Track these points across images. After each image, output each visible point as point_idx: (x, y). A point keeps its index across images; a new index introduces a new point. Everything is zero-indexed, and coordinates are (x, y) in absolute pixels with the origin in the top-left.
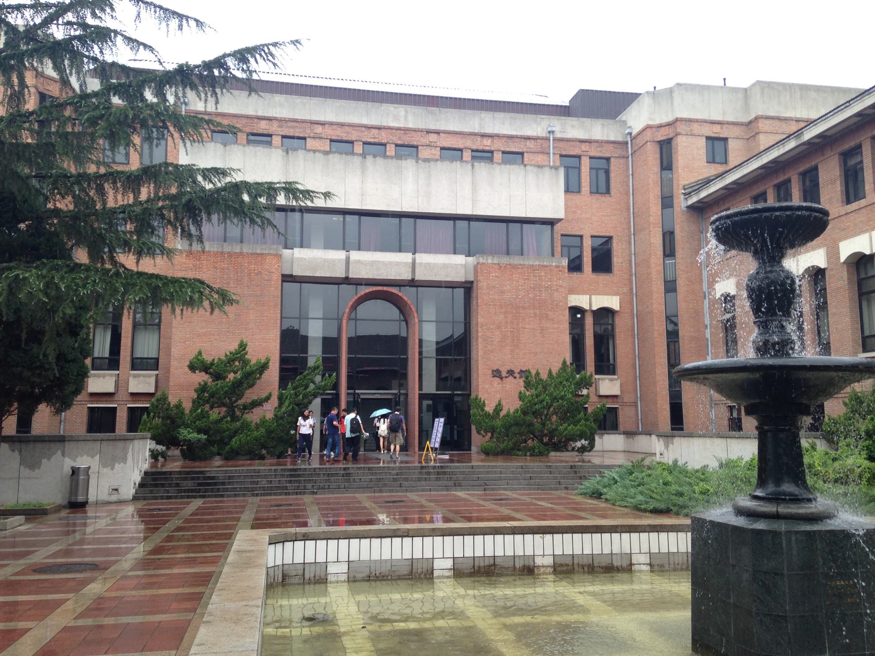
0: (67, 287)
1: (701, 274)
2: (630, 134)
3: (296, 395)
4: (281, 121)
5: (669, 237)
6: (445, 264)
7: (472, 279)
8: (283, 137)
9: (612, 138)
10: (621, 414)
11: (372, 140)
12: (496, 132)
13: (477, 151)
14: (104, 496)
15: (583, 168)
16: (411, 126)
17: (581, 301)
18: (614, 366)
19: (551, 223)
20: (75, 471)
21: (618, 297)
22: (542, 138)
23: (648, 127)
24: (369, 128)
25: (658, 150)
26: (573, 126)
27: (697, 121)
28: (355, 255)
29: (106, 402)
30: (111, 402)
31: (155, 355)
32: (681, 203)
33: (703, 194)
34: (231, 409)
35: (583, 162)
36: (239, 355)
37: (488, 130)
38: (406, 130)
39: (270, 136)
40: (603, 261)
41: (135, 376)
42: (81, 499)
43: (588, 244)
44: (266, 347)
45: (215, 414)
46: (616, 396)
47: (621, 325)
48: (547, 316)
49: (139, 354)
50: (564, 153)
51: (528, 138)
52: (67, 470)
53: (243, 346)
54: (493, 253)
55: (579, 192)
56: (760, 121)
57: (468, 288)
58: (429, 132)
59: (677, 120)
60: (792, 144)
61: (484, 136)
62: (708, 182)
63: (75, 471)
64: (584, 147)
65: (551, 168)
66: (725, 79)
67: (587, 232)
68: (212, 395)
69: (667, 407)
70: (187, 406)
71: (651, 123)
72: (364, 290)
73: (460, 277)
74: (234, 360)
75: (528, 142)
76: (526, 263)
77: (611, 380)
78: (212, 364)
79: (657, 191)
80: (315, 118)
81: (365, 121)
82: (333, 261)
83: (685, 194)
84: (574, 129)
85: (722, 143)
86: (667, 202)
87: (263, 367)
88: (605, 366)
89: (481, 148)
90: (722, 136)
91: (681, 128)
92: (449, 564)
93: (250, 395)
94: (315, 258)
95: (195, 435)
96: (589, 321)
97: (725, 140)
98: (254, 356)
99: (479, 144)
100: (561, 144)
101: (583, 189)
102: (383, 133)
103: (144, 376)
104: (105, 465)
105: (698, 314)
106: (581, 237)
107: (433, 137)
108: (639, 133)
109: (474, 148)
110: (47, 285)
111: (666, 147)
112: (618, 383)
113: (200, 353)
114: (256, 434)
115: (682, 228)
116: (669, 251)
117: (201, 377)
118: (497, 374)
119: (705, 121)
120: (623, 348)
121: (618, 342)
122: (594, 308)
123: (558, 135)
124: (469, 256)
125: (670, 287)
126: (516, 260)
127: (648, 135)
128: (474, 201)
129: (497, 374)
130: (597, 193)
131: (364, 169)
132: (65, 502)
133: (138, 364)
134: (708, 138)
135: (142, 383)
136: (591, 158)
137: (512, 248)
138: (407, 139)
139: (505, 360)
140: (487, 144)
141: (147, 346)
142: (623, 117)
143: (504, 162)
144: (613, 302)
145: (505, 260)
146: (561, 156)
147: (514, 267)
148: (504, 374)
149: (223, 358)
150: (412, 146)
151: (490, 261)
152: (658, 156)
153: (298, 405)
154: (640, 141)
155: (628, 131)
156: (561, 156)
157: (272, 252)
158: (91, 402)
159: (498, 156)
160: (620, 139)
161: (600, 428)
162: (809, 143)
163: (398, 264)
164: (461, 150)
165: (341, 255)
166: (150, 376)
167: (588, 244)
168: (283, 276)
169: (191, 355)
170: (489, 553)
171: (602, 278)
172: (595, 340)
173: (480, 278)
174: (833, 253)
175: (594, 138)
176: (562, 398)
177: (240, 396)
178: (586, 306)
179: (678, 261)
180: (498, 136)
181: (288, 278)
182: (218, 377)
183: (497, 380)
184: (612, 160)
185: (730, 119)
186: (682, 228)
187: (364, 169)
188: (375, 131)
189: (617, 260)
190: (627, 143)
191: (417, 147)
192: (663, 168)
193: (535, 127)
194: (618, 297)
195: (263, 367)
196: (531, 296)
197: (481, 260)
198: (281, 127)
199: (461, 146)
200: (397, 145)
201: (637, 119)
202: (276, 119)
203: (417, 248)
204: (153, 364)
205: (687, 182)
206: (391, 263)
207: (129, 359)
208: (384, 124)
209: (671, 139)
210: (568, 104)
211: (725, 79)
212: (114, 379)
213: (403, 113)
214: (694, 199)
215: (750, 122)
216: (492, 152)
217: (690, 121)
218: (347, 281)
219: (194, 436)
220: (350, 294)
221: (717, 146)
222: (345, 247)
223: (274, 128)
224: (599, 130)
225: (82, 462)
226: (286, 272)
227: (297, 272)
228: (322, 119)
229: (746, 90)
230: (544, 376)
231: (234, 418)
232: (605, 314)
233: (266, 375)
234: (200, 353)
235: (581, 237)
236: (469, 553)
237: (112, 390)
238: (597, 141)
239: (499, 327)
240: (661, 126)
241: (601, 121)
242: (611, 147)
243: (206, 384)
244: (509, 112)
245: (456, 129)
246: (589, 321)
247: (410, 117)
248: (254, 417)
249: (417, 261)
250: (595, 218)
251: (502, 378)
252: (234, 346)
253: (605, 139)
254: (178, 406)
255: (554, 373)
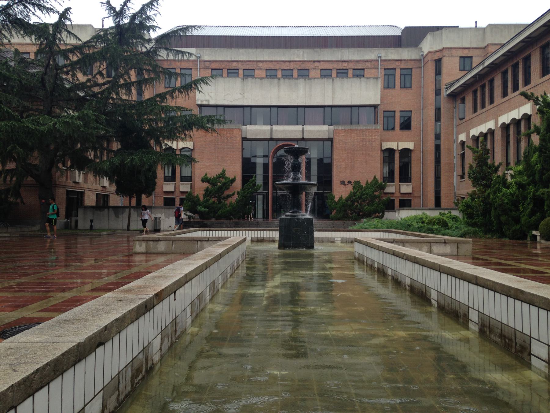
0: (146, 160)
1: (453, 130)
2: (423, 55)
3: (244, 193)
4: (242, 62)
5: (438, 110)
6: (318, 130)
7: (332, 137)
8: (244, 70)
9: (413, 58)
10: (412, 202)
11: (286, 68)
12: (350, 59)
13: (340, 69)
14: (166, 228)
15: (396, 75)
16: (306, 59)
17: (393, 145)
18: (410, 178)
19: (375, 107)
20: (156, 218)
21: (413, 143)
22: (374, 61)
23: (430, 52)
24: (284, 62)
25: (435, 64)
26: (392, 53)
27: (455, 48)
28: (275, 128)
29: (171, 195)
30: (173, 195)
31: (190, 175)
32: (445, 93)
33: (452, 89)
34: (219, 198)
35: (397, 72)
36: (223, 175)
37: (346, 58)
38: (303, 62)
39: (238, 69)
40: (406, 125)
41: (182, 184)
42: (158, 228)
43: (398, 115)
44: (235, 171)
45: (212, 200)
46: (410, 193)
47: (414, 157)
48: (369, 154)
49: (183, 175)
50: (386, 67)
51: (367, 61)
52: (153, 219)
53: (224, 171)
54: (345, 123)
55: (394, 87)
56: (489, 46)
57: (331, 140)
58: (314, 62)
59: (443, 49)
60: (481, 68)
61: (343, 61)
62: (458, 80)
63: (156, 218)
64: (398, 63)
65: (374, 78)
66: (476, 22)
67: (398, 109)
68: (210, 193)
69: (433, 198)
70: (201, 198)
71: (431, 50)
72: (280, 144)
73: (326, 136)
74: (220, 178)
75: (367, 63)
76: (359, 128)
77: (407, 185)
78: (210, 179)
79: (433, 87)
80: (258, 59)
81: (283, 59)
82: (265, 130)
83: (446, 88)
84: (392, 54)
85: (470, 59)
86: (438, 92)
87: (233, 180)
88: (405, 177)
89: (341, 68)
90: (469, 55)
91: (446, 53)
92: (250, 239)
93: (226, 193)
94: (258, 130)
95: (203, 209)
96: (397, 155)
97: (471, 57)
98: (229, 175)
99: (340, 66)
100: (385, 63)
101: (396, 86)
102: (292, 64)
103: (186, 184)
104: (166, 217)
105: (450, 151)
106: (395, 111)
107: (317, 64)
108: (426, 55)
109: (338, 68)
110: (141, 160)
111: (438, 63)
112: (411, 187)
113: (206, 174)
114: (228, 209)
115: (445, 106)
116: (438, 119)
117: (206, 185)
118: (343, 183)
119: (460, 48)
120: (415, 169)
121: (412, 166)
122: (400, 149)
123: (383, 58)
124: (331, 125)
125: (438, 137)
126: (354, 127)
127: (429, 57)
128: (333, 98)
129: (343, 183)
130: (405, 87)
131: (279, 85)
132: (153, 230)
133: (184, 179)
134: (461, 57)
135: (185, 187)
136: (401, 69)
137: (353, 120)
138: (304, 66)
139: (347, 176)
140: (345, 65)
141: (186, 172)
142: (420, 46)
143: (354, 76)
144: (410, 145)
145: (348, 127)
146: (385, 69)
147: (352, 130)
148: (346, 183)
149: (215, 176)
150: (306, 70)
151: (340, 128)
152: (434, 68)
153: (245, 197)
154: (426, 60)
155: (421, 54)
156: (385, 69)
157: (237, 128)
158: (165, 195)
159: (350, 72)
160: (418, 58)
161: (386, 209)
162: (487, 66)
163: (295, 131)
164: (331, 70)
165: (268, 128)
166: (188, 184)
167: (398, 115)
168: (243, 138)
169: (203, 176)
170: (262, 236)
171: (406, 132)
172: (399, 164)
173: (335, 136)
174: (497, 123)
175: (403, 58)
176: (367, 194)
177: (223, 193)
178: (395, 148)
179: (442, 123)
180: (351, 61)
181: (244, 139)
182: (213, 184)
183: (343, 186)
184: (413, 70)
185: (474, 45)
186: (445, 106)
187: (279, 85)
188: (288, 63)
189: (413, 124)
190: (421, 60)
191: (309, 70)
192: (436, 74)
193: (370, 54)
194: (413, 143)
195: (233, 180)
196: (361, 144)
197: (336, 128)
198: (242, 65)
199: (331, 68)
200: (298, 70)
201: (428, 45)
202: (240, 61)
203: (306, 123)
204: (188, 179)
205: (448, 82)
206: (292, 131)
207: (179, 177)
208: (292, 59)
209: (441, 59)
210: (400, 34)
211: (476, 22)
212: (190, 186)
213: (301, 53)
214: (449, 92)
215: (485, 47)
216: (348, 70)
217: (451, 48)
218: (271, 139)
219: (203, 209)
220: (273, 146)
221: (465, 61)
222: (271, 125)
223: (239, 66)
224: (406, 54)
225: (158, 216)
226: (244, 136)
227: (249, 136)
228: (262, 59)
229: (484, 29)
230: (364, 185)
231: (220, 202)
232: (406, 152)
233: (234, 184)
234: (206, 174)
235: (395, 111)
236: (256, 236)
237: (173, 190)
238: (405, 60)
239: (344, 160)
240: (436, 52)
241: (408, 49)
242: (412, 63)
243: (208, 187)
244: (356, 47)
245: (329, 59)
246: (397, 155)
247: (305, 55)
248: (228, 202)
249: (305, 129)
250: (401, 101)
251: (345, 185)
252: (220, 171)
253: (409, 58)
254: (197, 197)
255: (369, 182)
